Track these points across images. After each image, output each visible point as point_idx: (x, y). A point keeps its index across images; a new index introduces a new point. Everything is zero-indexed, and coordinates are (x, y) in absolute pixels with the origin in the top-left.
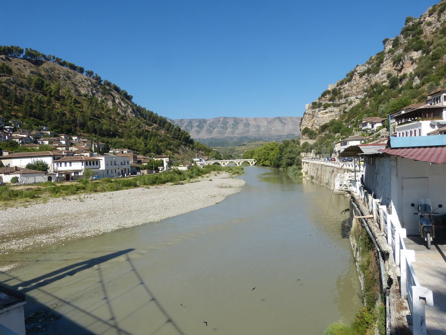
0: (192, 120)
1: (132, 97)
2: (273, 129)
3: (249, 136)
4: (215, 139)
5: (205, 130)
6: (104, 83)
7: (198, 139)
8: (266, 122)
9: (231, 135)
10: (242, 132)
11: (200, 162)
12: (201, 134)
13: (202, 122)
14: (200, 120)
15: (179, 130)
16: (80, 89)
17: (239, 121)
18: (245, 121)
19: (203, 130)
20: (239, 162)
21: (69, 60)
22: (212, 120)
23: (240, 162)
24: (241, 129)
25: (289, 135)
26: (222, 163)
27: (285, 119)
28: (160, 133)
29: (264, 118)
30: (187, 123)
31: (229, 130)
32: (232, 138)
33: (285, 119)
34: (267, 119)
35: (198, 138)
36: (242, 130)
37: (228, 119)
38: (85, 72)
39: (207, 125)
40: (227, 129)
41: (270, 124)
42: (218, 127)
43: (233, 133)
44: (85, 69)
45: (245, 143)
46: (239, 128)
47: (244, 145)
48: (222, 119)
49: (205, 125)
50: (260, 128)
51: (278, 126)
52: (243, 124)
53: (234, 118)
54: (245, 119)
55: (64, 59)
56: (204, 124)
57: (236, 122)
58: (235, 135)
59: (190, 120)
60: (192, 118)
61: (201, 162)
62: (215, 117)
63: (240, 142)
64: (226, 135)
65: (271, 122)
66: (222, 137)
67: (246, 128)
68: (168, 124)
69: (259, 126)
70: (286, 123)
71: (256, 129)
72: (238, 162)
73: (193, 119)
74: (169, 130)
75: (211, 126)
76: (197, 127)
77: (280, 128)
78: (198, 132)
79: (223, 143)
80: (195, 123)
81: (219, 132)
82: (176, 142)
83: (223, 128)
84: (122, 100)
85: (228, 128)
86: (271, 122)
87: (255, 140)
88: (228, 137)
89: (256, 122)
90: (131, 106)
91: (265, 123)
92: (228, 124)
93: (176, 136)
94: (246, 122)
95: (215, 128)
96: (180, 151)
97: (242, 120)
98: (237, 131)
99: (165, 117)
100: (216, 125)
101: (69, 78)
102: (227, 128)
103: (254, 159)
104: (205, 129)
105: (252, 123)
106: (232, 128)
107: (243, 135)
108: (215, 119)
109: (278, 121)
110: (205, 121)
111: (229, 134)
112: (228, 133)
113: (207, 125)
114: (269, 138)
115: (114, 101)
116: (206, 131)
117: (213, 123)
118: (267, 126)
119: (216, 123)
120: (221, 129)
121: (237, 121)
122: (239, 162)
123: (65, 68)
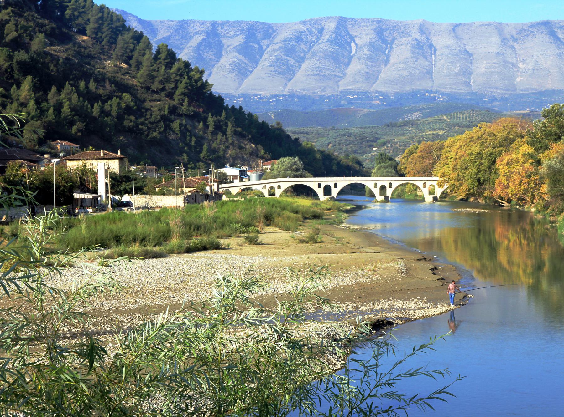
0: (223, 24)
2: (521, 66)
3: (431, 92)
4: (302, 98)
5: (267, 63)
7: (244, 95)
8: (496, 39)
10: (405, 73)
11: (241, 180)
12: (251, 77)
13: (259, 36)
14: (253, 25)
15: (172, 57)
17: (395, 34)
18: (418, 36)
19: (261, 63)
20: (383, 188)
22: (296, 27)
23: (275, 186)
24: (401, 66)
26: (319, 186)
29: (490, 24)
30: (202, 37)
31: (355, 67)
32: (365, 97)
34: (499, 28)
35: (241, 91)
36: (404, 69)
37: (353, 25)
39: (276, 47)
40: (348, 64)
41: (513, 47)
42: (314, 54)
46: (392, 60)
48: (332, 26)
49: (268, 46)
50: (471, 63)
52: (409, 47)
53: (379, 21)
54: (417, 26)
56: (265, 42)
58: (379, 86)
59: (214, 24)
60: (219, 18)
61: (246, 182)
62: (307, 18)
64: (343, 86)
65: (515, 40)
67: (422, 61)
68: (127, 36)
69: (470, 55)
71: (458, 65)
72: (322, 186)
73: (228, 22)
74: (130, 58)
76: (240, 54)
77: (549, 63)
80: (233, 37)
83: (334, 58)
85: (354, 61)
88: (350, 93)
89: (458, 38)
92: (353, 45)
93: (156, 86)
94: (423, 38)
95: (303, 60)
99: (120, 8)
100: (310, 48)
102: (350, 58)
103: (438, 178)
104: (267, 60)
107: (408, 88)
108: (304, 23)
111: (355, 82)
113: (276, 47)
116: (272, 69)
117: (298, 39)
118: (498, 54)
119: (310, 38)
121: (387, 34)
122: (383, 188)
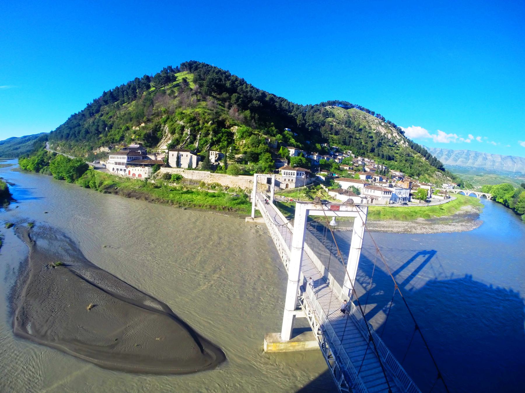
1: (405, 132)
2: (505, 165)
4: (459, 166)
6: (387, 122)
9: (472, 166)
10: (481, 164)
13: (451, 152)
16: (372, 126)
21: (366, 107)
25: (517, 172)
27: (515, 158)
28: (422, 161)
30: (439, 151)
32: (472, 168)
33: (515, 158)
38: (375, 114)
40: (469, 160)
43: (473, 163)
44: (376, 113)
45: (482, 174)
46: (478, 160)
47: (481, 176)
48: (466, 151)
51: (509, 163)
55: (363, 106)
56: (452, 154)
57: (477, 155)
58: (475, 166)
63: (479, 171)
64: (467, 164)
65: (504, 159)
66: (464, 166)
69: (494, 161)
70: (516, 161)
75: (457, 156)
78: (446, 159)
79: (465, 171)
81: (462, 162)
82: (433, 168)
83: (466, 158)
84: (398, 134)
86: (504, 159)
87: (490, 172)
89: (492, 157)
90: (403, 139)
91: (499, 160)
96: (434, 176)
97: (481, 154)
98: (477, 163)
101: (365, 118)
102: (469, 159)
104: (452, 158)
105: (489, 157)
106: (473, 159)
109: (509, 159)
110: (453, 151)
112: (469, 163)
114: (501, 172)
115: (392, 134)
117: (459, 154)
118: (500, 162)
120: (465, 160)
123: (364, 112)
